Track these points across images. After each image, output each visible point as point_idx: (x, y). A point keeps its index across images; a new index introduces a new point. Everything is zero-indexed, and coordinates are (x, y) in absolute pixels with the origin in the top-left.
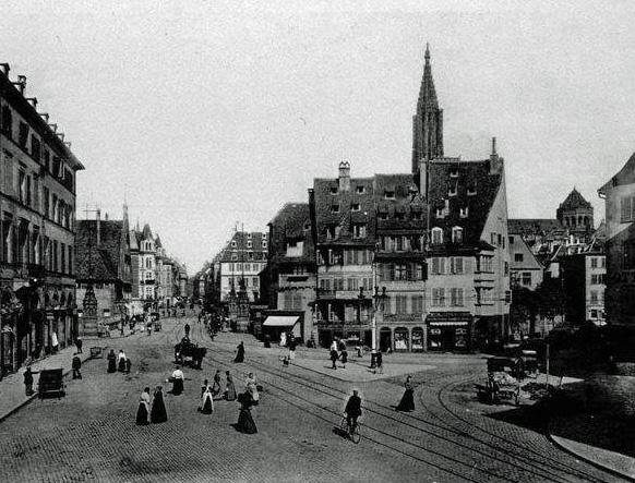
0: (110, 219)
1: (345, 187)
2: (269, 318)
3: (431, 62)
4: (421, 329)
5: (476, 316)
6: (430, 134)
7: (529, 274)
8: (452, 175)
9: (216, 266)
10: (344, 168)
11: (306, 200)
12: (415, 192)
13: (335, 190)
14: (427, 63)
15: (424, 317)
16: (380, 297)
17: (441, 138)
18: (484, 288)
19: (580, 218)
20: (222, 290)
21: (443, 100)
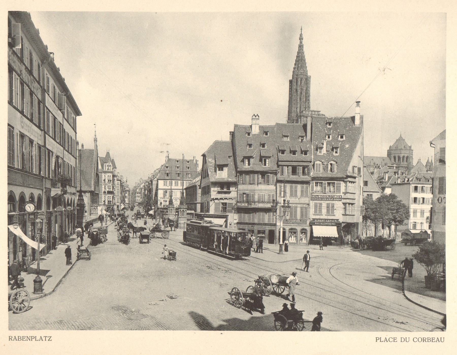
0: (85, 147)
1: (255, 130)
2: (419, 232)
3: (304, 42)
4: (306, 230)
5: (343, 222)
6: (301, 93)
7: (371, 195)
8: (328, 126)
9: (154, 183)
10: (256, 117)
11: (227, 138)
12: (302, 137)
13: (249, 134)
14: (301, 42)
15: (308, 222)
16: (287, 207)
17: (309, 96)
18: (349, 204)
19: (403, 157)
20: (159, 198)
21: (311, 70)
